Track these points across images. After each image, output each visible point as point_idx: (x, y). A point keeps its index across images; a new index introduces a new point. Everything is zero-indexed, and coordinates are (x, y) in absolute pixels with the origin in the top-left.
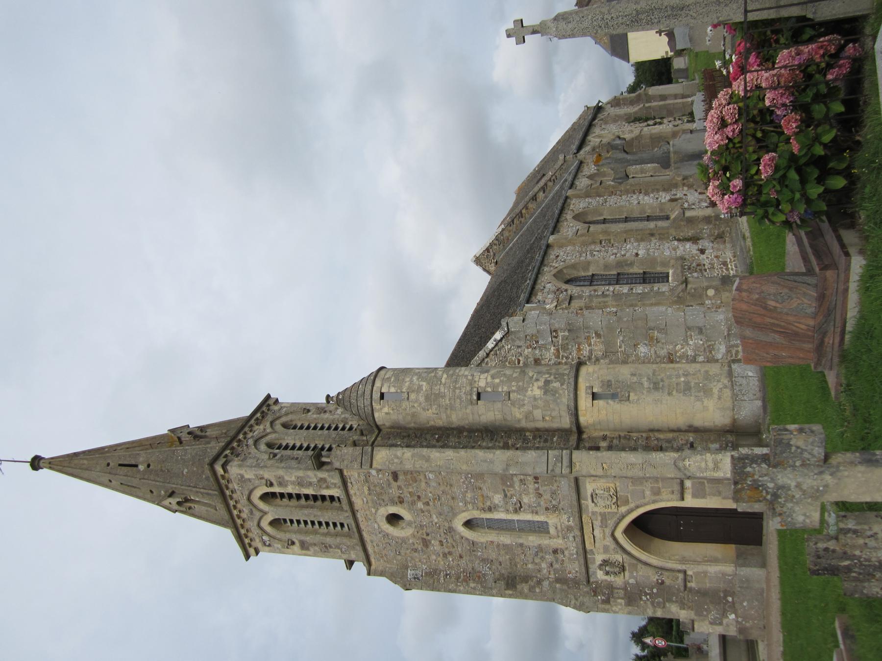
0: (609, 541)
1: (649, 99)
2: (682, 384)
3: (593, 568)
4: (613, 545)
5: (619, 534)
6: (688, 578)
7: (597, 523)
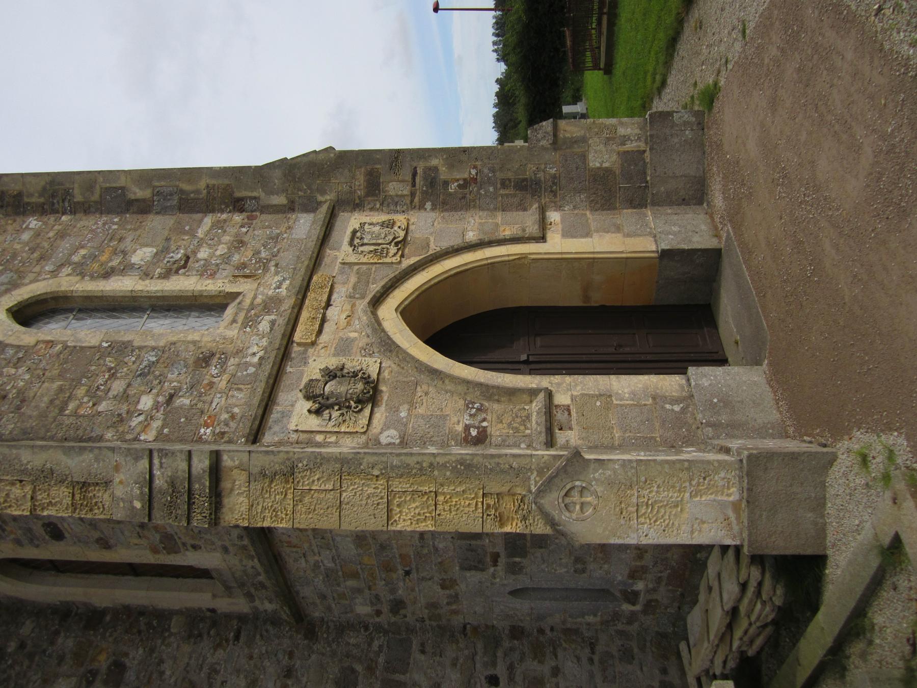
6: (560, 416)
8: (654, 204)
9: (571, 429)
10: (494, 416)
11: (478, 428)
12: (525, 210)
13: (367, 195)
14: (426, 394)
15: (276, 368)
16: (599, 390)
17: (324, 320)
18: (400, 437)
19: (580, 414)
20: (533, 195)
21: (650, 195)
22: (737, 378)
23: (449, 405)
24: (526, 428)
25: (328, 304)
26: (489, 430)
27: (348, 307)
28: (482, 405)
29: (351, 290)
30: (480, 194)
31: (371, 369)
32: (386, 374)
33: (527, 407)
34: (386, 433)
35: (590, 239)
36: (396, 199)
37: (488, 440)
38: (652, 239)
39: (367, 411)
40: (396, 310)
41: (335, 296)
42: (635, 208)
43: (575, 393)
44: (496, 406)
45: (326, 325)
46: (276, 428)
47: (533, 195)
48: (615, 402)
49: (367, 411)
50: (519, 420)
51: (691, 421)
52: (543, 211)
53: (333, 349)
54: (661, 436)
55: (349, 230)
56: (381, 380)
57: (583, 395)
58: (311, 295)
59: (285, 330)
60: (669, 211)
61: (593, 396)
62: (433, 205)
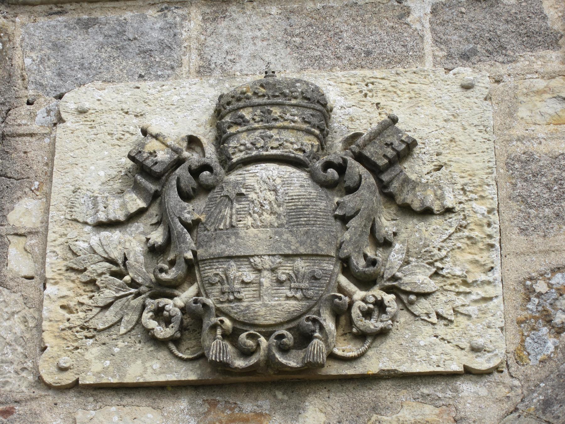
31: (425, 335)
46: (83, 45)
56: (367, 395)
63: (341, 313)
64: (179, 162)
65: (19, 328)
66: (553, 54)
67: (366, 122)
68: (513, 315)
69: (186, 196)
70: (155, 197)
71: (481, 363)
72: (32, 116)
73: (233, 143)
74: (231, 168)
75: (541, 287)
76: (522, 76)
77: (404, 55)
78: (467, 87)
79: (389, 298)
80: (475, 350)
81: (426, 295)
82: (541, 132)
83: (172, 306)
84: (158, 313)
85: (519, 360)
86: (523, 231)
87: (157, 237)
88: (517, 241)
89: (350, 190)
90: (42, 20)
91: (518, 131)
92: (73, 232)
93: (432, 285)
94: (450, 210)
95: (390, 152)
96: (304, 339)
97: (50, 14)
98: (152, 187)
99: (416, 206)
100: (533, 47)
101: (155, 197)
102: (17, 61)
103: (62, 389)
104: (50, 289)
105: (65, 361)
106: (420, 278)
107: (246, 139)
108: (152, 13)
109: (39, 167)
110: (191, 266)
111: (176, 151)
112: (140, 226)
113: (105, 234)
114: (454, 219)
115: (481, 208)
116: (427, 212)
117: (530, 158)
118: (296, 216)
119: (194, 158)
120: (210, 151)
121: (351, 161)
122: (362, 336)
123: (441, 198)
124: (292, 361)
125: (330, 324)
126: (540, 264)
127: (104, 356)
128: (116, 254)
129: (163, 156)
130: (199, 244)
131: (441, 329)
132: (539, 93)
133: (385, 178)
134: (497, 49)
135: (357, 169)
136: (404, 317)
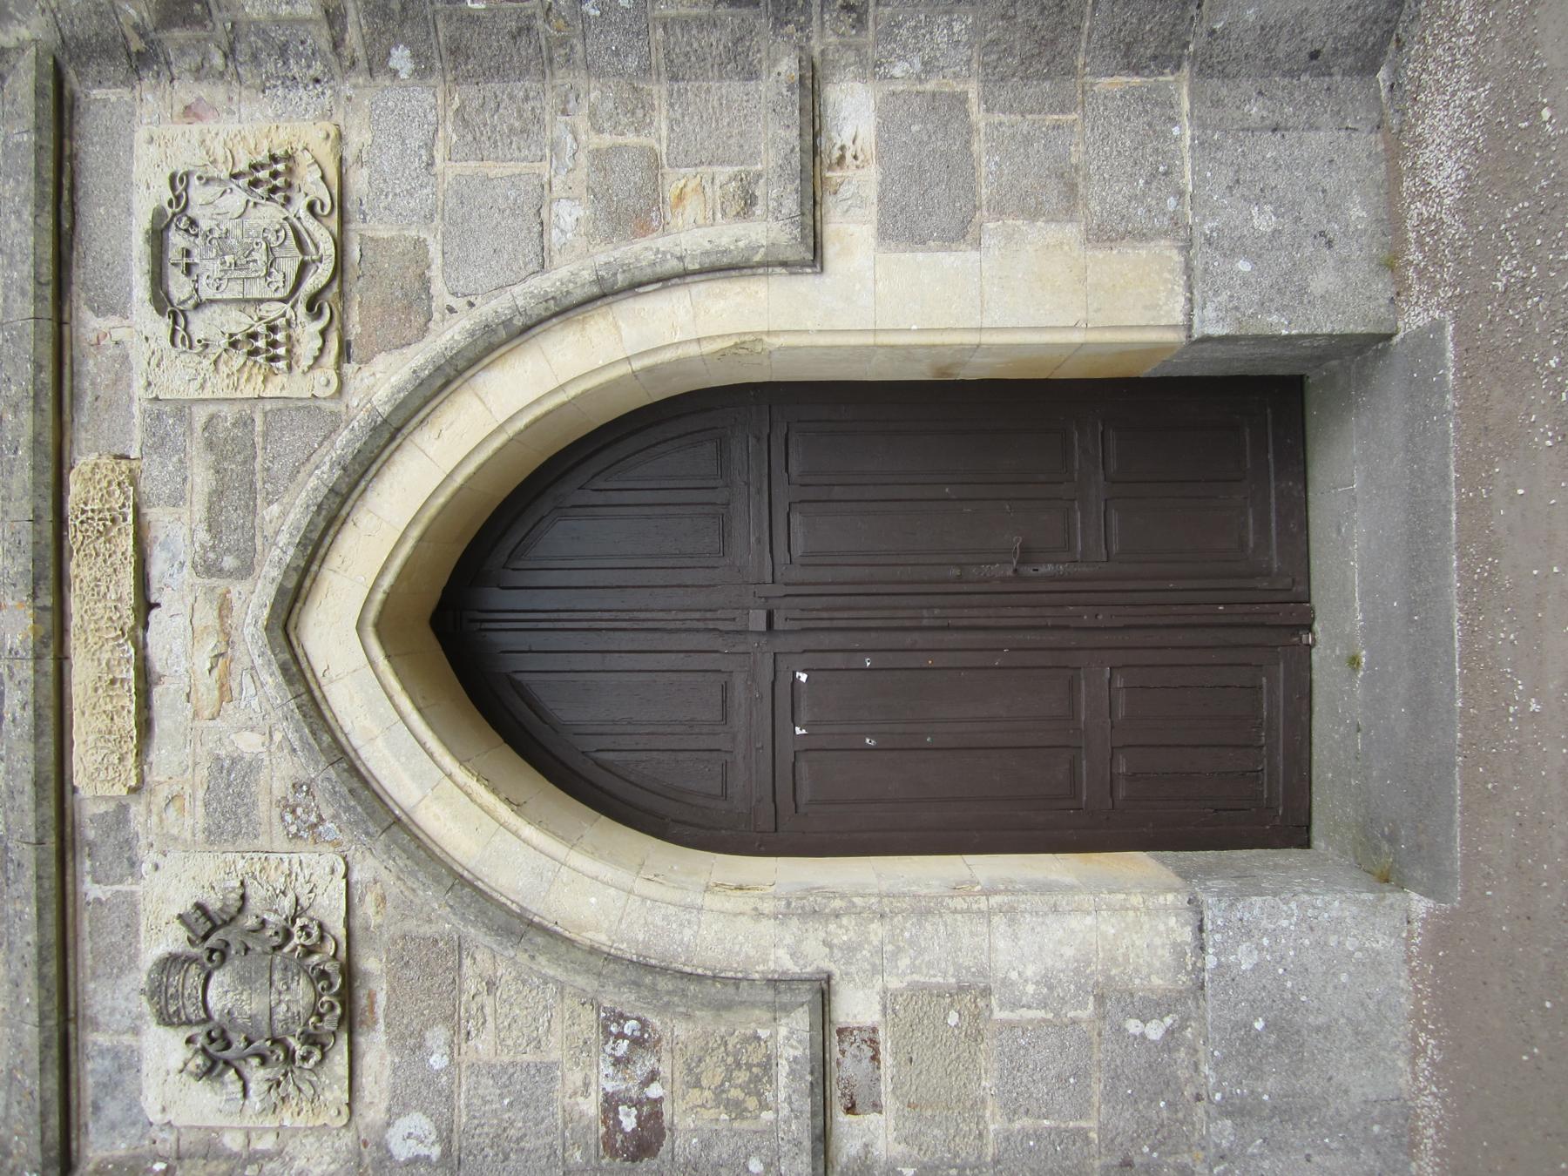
0: (257, 728)
1: (16, 439)
2: (997, 117)
3: (115, 1001)
4: (280, 760)
5: (337, 635)
6: (849, 1066)
7: (178, 533)
8: (1206, 68)
9: (877, 1107)
10: (679, 1062)
11: (637, 1104)
12: (752, 75)
13: (166, 20)
14: (491, 985)
15: (51, 917)
16: (958, 967)
17: (145, 679)
18: (440, 1139)
19: (903, 1058)
20: (780, 23)
21: (1202, 29)
22: (1333, 940)
23: (557, 1026)
24: (764, 1106)
25: (145, 605)
26: (666, 1108)
27: (207, 616)
28: (644, 1024)
29: (203, 535)
30: (585, 18)
31: (322, 900)
32: (368, 910)
33: (763, 1033)
34: (403, 1125)
35: (974, 255)
36: (279, 36)
37: (666, 1143)
38: (1177, 258)
39: (339, 1059)
40: (359, 628)
41: (156, 569)
42: (1137, 70)
43: (894, 983)
44: (682, 1030)
45: (157, 692)
46: (112, 1110)
47: (780, 23)
48: (999, 1014)
49: (339, 1059)
50: (742, 1076)
51: (1183, 1074)
52: (811, 85)
53: (200, 810)
54: (1102, 1128)
55: (141, 223)
56: (358, 933)
57: (916, 989)
58: (80, 570)
59: (38, 761)
60: (1255, 110)
61: (938, 993)
62: (416, 56)
63: (309, 951)
64: (204, 1050)
65: (311, 1139)
66: (133, 809)
67: (182, 933)
68: (311, 848)
69: (228, 1045)
70: (227, 1063)
71: (341, 869)
72: (164, 1141)
73: (193, 1017)
74: (209, 1018)
75: (293, 829)
76: (148, 831)
77: (131, 904)
78: (157, 867)
79: (299, 922)
80: (333, 871)
81: (297, 900)
82: (189, 822)
83: (300, 1050)
84: (305, 1058)
85: (339, 844)
86: (256, 837)
87: (255, 1061)
88: (263, 842)
89: (227, 944)
90: (92, 1137)
91: (188, 836)
92: (248, 1112)
93: (291, 895)
94: (242, 883)
95: (202, 920)
96: (324, 975)
97: (87, 1133)
98: (221, 1066)
99: (239, 904)
100: (127, 821)
101: (227, 1063)
102: (122, 1153)
103: (351, 1112)
104: (287, 1123)
105: (334, 1112)
106: (287, 904)
107: (190, 1010)
108: (89, 1066)
109: (201, 1135)
110: (275, 1041)
111: (196, 1052)
112: (246, 1072)
113: (251, 1092)
114: (248, 881)
115: (241, 863)
116: (243, 897)
117: (208, 831)
118: (244, 980)
119: (201, 1041)
120: (196, 1030)
121: (208, 944)
122: (322, 938)
123: (234, 889)
124: (339, 981)
125: (315, 958)
126: (278, 828)
127: (332, 1090)
128: (266, 1087)
129: (199, 1060)
130: (261, 1037)
131: (319, 891)
132: (161, 821)
133: (219, 922)
134: (128, 844)
135: (213, 941)
136: (311, 913)
